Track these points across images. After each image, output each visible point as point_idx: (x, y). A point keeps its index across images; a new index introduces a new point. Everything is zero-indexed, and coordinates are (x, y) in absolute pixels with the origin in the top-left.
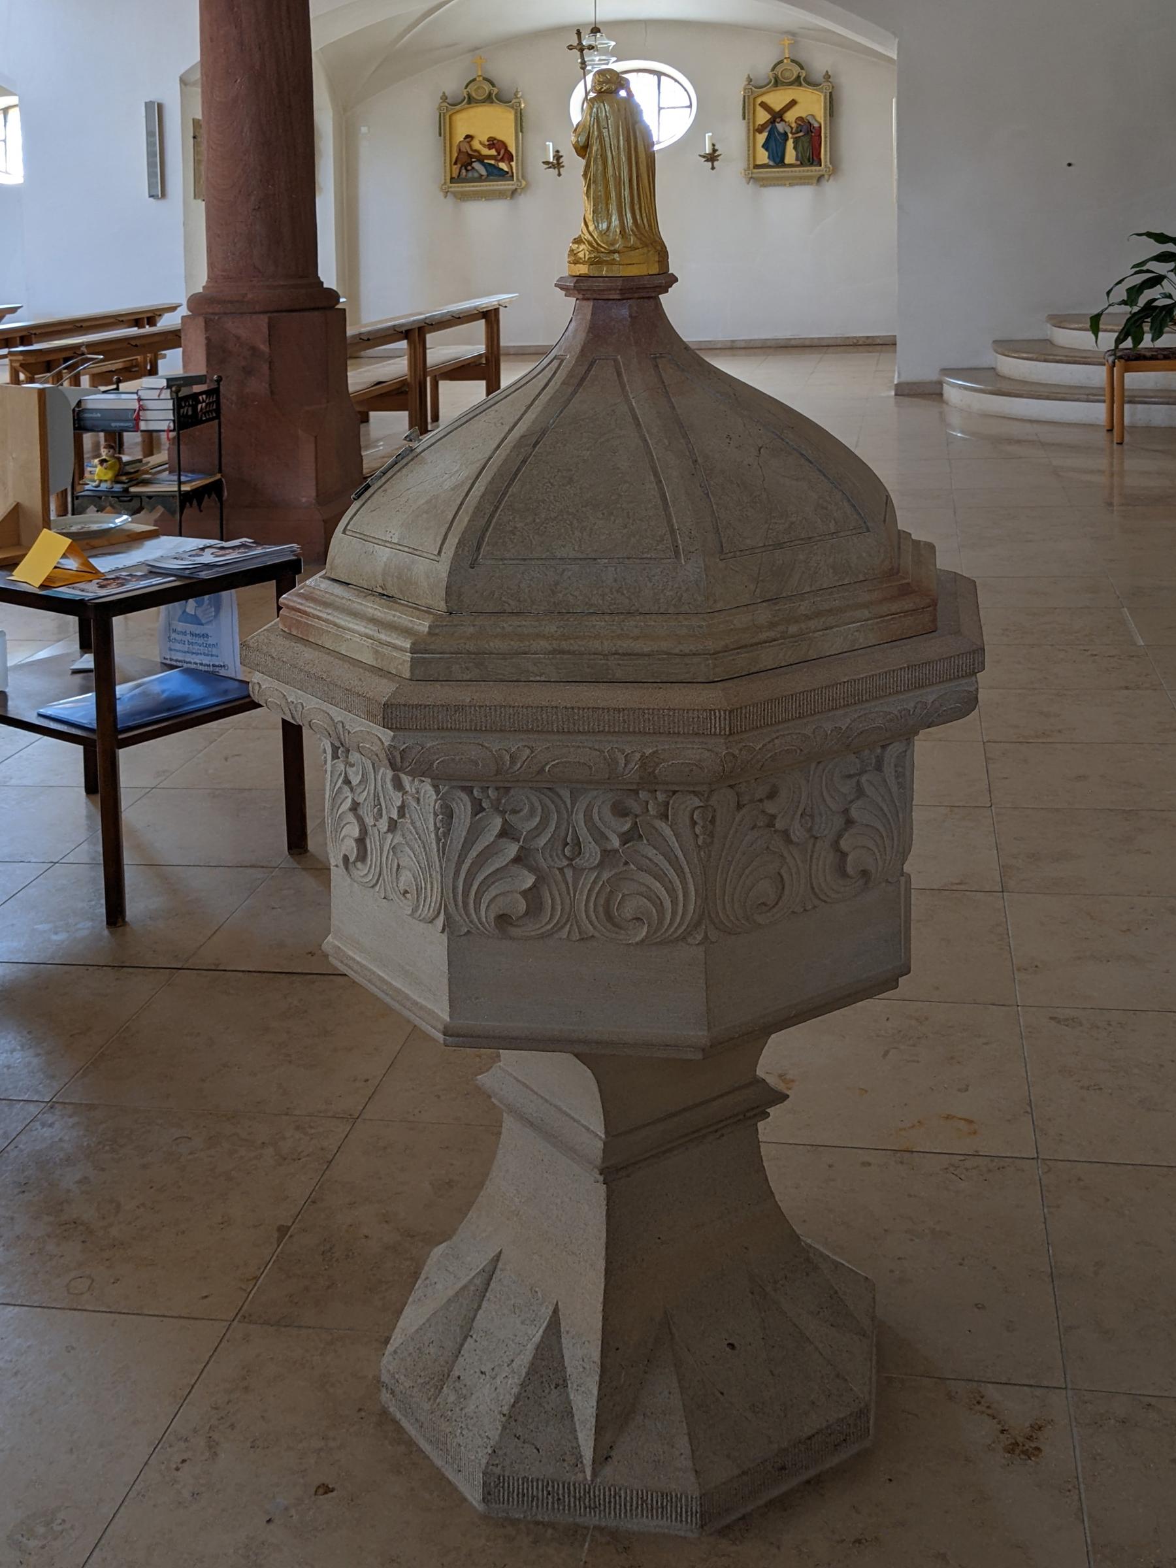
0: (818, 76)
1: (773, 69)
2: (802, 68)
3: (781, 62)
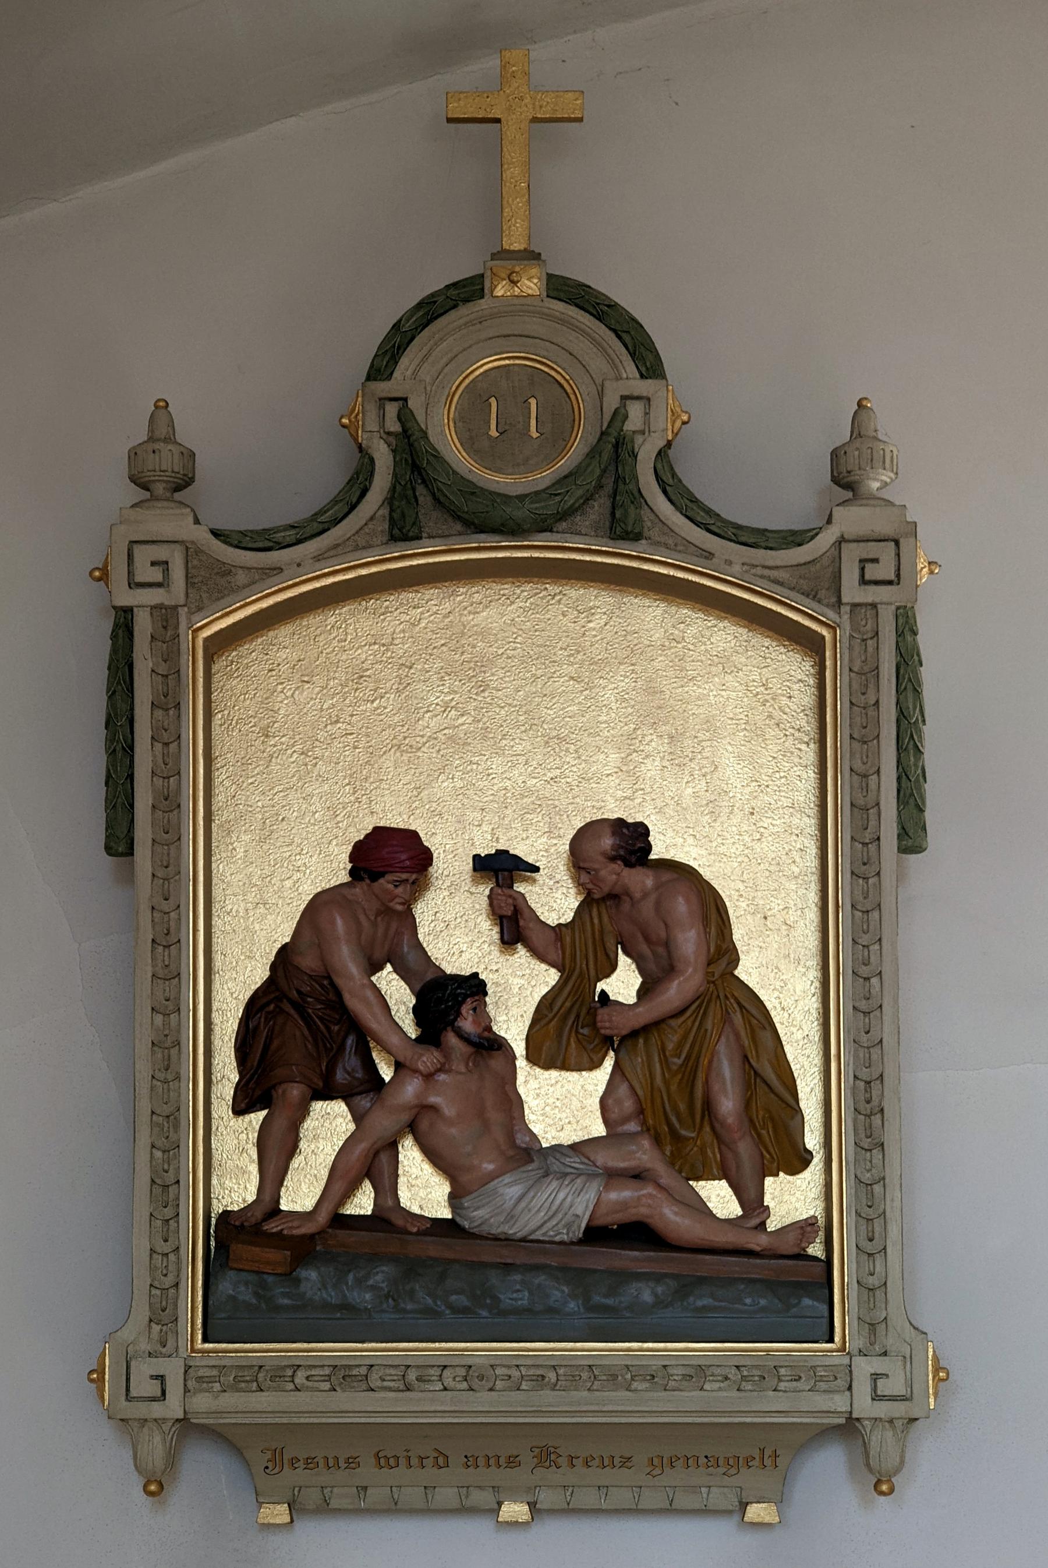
0: (738, 414)
3: (469, 290)
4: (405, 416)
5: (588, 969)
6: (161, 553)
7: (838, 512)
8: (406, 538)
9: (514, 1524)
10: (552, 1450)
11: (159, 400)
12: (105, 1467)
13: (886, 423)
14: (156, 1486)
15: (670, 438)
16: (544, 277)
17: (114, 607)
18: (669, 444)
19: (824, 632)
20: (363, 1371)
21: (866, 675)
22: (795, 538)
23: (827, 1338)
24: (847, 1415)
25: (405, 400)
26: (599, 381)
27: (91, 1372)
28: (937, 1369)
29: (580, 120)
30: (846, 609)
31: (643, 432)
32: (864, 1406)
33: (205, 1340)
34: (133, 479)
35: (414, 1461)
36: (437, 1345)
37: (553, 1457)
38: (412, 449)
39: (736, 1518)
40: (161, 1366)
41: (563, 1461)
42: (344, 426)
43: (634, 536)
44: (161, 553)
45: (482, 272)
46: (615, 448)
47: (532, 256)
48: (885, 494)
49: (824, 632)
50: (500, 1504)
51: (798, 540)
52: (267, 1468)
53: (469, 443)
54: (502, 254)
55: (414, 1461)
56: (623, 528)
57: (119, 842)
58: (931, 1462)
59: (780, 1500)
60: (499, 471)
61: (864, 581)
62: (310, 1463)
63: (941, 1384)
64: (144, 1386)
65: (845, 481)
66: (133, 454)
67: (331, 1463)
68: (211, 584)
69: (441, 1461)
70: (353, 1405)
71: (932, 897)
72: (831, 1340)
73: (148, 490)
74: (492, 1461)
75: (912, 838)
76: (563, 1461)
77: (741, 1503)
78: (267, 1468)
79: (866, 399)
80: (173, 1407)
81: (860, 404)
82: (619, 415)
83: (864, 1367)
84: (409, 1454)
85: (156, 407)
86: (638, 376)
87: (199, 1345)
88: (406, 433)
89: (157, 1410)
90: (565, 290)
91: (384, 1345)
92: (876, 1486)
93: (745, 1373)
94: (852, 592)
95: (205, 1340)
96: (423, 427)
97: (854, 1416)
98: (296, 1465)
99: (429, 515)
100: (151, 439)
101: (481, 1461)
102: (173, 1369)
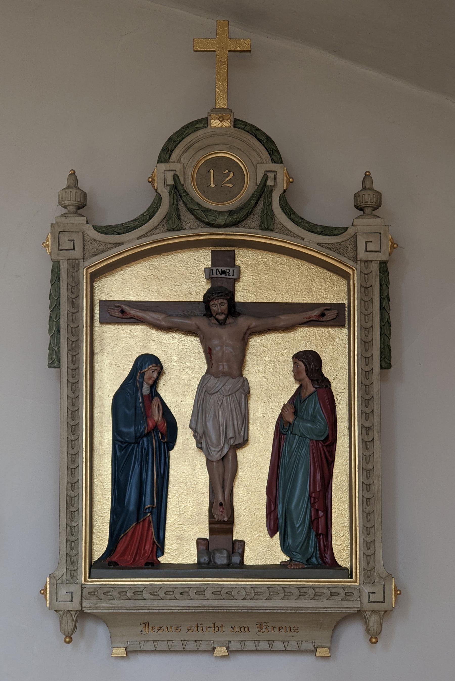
0: (329, 204)
1: (165, 155)
2: (275, 154)
3: (201, 124)
5: (237, 415)
6: (73, 236)
10: (265, 624)
14: (69, 638)
15: (285, 188)
16: (233, 120)
18: (285, 191)
21: (365, 329)
22: (158, 200)
27: (400, 594)
28: (396, 591)
29: (250, 51)
30: (359, 262)
32: (366, 605)
33: (90, 578)
34: (356, 207)
40: (72, 588)
44: (73, 236)
45: (207, 117)
47: (228, 110)
51: (336, 232)
52: (142, 631)
53: (204, 192)
54: (215, 110)
56: (268, 224)
57: (54, 362)
58: (399, 631)
61: (366, 251)
63: (398, 596)
66: (356, 196)
75: (386, 362)
77: (315, 648)
78: (142, 631)
80: (75, 605)
84: (203, 626)
86: (270, 161)
89: (70, 606)
90: (237, 123)
94: (362, 254)
95: (90, 578)
96: (182, 183)
100: (364, 188)
102: (76, 589)
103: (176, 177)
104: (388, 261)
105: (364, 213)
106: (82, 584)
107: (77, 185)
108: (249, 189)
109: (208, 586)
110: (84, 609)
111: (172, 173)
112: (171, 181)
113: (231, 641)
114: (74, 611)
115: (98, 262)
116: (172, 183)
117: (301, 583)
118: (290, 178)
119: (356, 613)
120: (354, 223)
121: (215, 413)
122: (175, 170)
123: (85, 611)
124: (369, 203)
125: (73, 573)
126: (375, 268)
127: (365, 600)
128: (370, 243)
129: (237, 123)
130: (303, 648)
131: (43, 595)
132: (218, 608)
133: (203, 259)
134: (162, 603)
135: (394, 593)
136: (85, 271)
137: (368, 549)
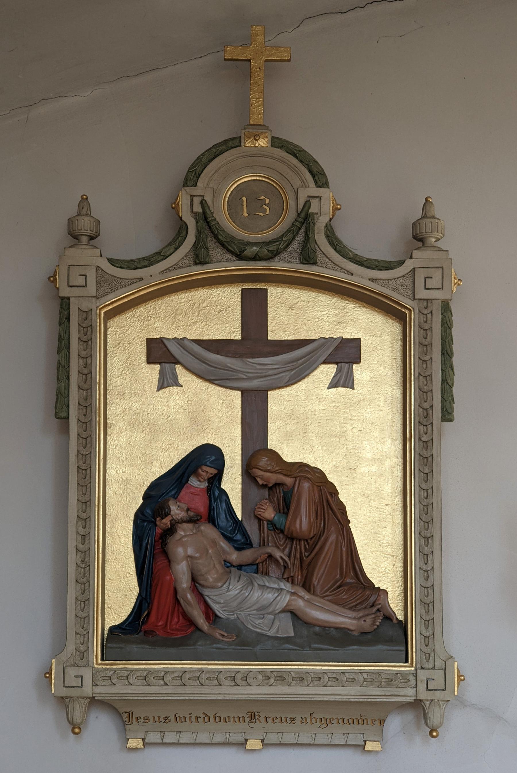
0: (369, 231)
2: (320, 178)
3: (233, 143)
4: (203, 203)
7: (415, 253)
8: (202, 263)
9: (135, 749)
10: (257, 714)
11: (85, 195)
12: (46, 719)
13: (438, 210)
15: (331, 217)
17: (60, 297)
19: (407, 312)
20: (162, 674)
21: (425, 331)
23: (405, 661)
24: (414, 698)
25: (203, 196)
26: (295, 188)
29: (289, 61)
31: (317, 214)
32: (423, 695)
35: (193, 720)
36: (356, 664)
37: (257, 717)
38: (205, 218)
39: (361, 748)
41: (262, 719)
42: (173, 208)
43: (315, 263)
46: (305, 219)
48: (439, 244)
49: (407, 312)
50: (246, 740)
55: (193, 720)
58: (457, 724)
59: (380, 738)
60: (261, 231)
62: (146, 719)
63: (461, 682)
64: (71, 681)
65: (419, 239)
66: (70, 221)
67: (157, 719)
68: (106, 284)
69: (206, 718)
70: (193, 692)
71: (453, 442)
72: (407, 661)
73: (77, 239)
74: (340, 721)
75: (447, 415)
76: (262, 719)
79: (429, 197)
81: (426, 200)
82: (307, 204)
83: (422, 675)
85: (82, 198)
87: (100, 662)
88: (204, 212)
90: (277, 143)
91: (195, 662)
92: (431, 733)
93: (366, 677)
95: (102, 659)
97: (418, 698)
98: (275, 721)
99: (216, 252)
101: (335, 721)
103: (203, 203)
104: (451, 300)
105: (423, 244)
106: (416, 669)
107: (89, 211)
108: (289, 217)
109: (324, 672)
110: (94, 696)
111: (200, 199)
112: (198, 209)
113: (147, 732)
114: (427, 700)
115: (112, 300)
116: (200, 210)
117: (189, 666)
118: (338, 204)
119: (412, 702)
120: (413, 256)
121: (183, 474)
122: (203, 196)
123: (96, 698)
124: (83, 231)
125: (83, 655)
126: (436, 309)
127: (422, 687)
128: (430, 279)
129: (277, 143)
130: (166, 740)
131: (48, 679)
132: (132, 695)
133: (230, 297)
134: (286, 690)
135: (456, 680)
136: (98, 311)
137: (427, 628)
